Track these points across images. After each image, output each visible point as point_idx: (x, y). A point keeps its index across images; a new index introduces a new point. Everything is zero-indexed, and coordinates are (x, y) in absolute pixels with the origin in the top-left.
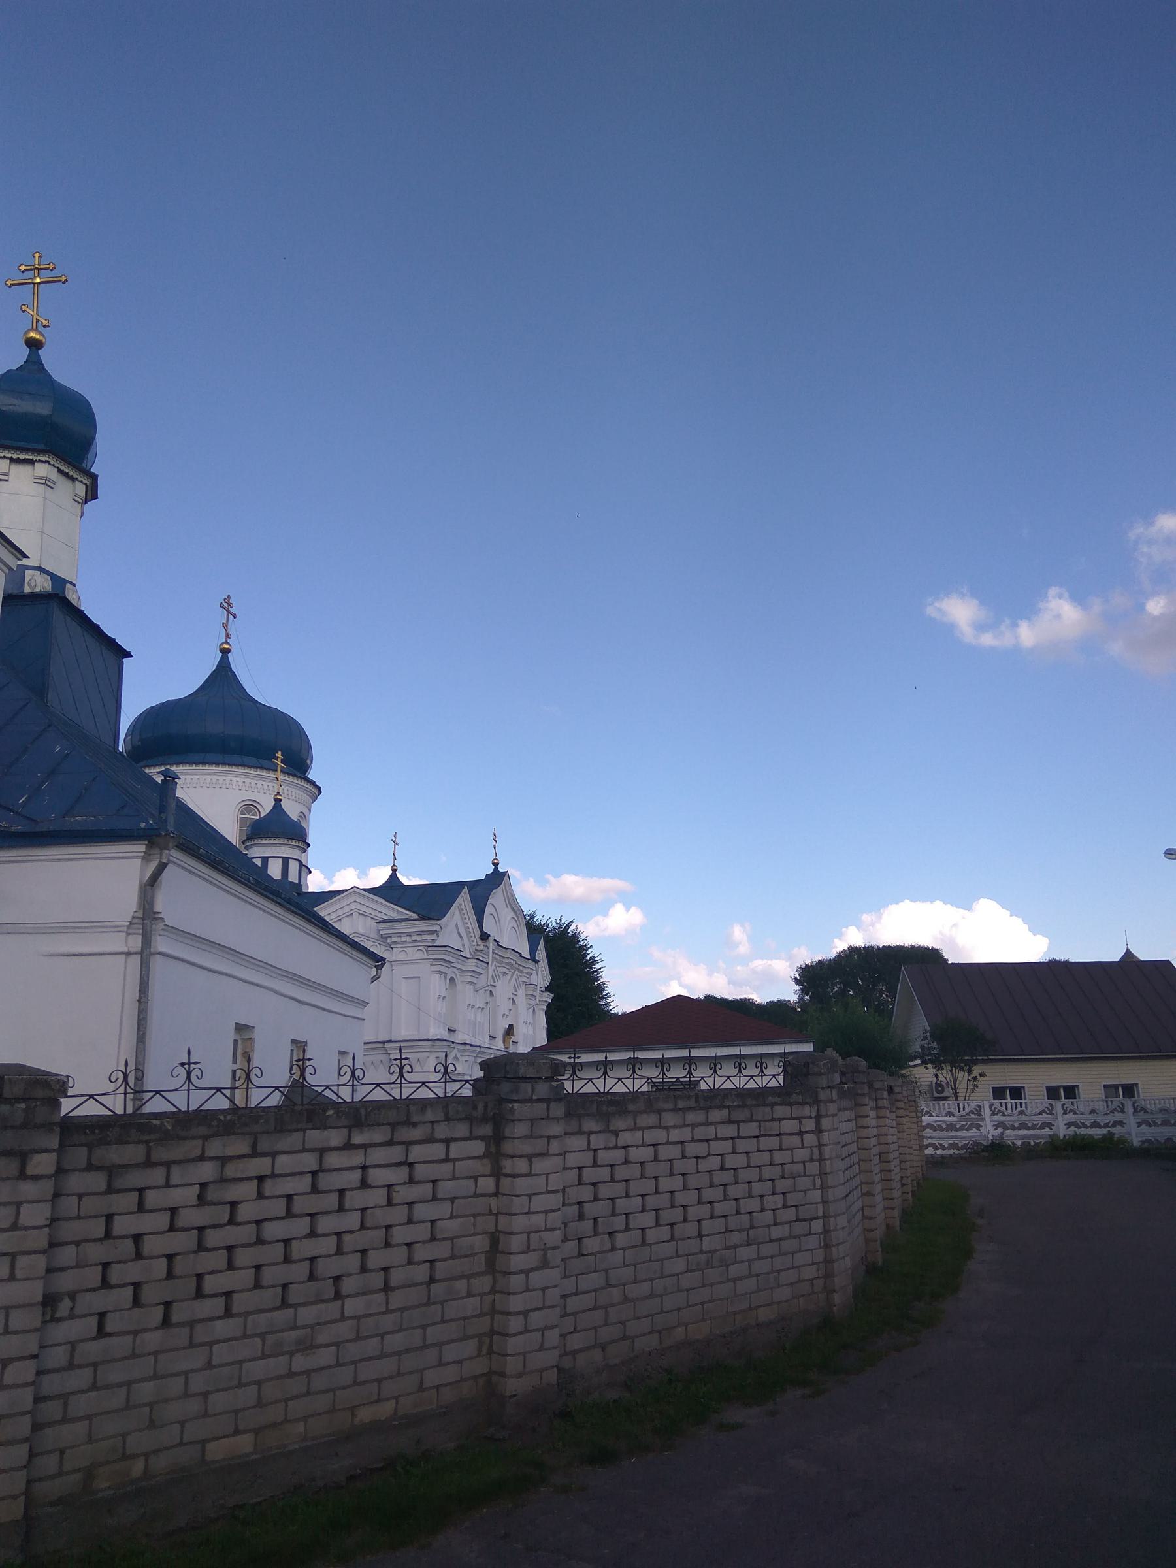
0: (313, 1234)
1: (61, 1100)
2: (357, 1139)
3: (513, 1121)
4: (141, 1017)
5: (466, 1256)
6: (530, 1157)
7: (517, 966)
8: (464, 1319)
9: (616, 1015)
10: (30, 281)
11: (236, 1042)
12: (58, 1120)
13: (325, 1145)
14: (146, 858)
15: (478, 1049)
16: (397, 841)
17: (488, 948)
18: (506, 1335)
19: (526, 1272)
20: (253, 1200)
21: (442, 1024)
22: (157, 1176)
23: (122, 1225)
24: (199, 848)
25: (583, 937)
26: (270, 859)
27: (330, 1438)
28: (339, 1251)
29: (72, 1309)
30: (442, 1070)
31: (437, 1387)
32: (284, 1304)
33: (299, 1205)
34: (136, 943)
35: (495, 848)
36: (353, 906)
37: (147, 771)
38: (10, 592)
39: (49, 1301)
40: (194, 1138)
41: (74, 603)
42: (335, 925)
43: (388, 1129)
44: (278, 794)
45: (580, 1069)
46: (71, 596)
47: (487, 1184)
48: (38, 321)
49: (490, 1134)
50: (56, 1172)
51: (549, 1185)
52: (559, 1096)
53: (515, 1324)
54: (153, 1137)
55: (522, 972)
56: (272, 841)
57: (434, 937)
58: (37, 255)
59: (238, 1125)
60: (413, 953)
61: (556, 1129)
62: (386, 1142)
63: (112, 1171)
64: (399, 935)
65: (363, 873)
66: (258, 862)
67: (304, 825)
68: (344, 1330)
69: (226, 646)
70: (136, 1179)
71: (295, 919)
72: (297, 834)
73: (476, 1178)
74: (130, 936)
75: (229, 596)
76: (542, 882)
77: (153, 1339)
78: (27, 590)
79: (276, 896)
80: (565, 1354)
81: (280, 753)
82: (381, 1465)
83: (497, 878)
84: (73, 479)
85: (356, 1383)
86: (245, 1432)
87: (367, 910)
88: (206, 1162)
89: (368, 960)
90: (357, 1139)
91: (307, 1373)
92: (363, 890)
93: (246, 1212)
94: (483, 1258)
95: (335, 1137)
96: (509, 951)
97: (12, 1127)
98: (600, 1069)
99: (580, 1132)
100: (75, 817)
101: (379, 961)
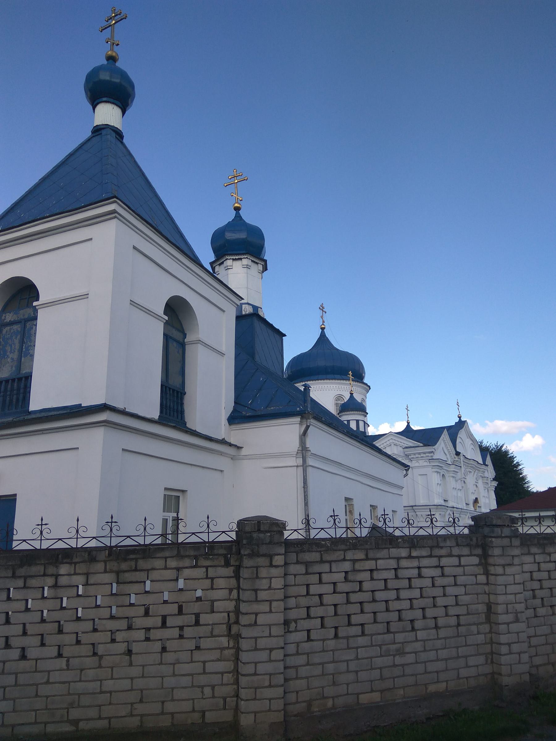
0: (398, 599)
1: (284, 532)
2: (414, 554)
3: (492, 547)
4: (305, 494)
5: (475, 614)
6: (504, 566)
7: (477, 468)
8: (477, 645)
9: (533, 492)
10: (233, 182)
11: (346, 506)
12: (283, 541)
13: (400, 556)
14: (301, 423)
15: (460, 510)
16: (408, 409)
17: (460, 459)
18: (501, 655)
19: (508, 624)
20: (369, 581)
21: (441, 497)
22: (325, 567)
23: (314, 589)
24: (322, 418)
25: (510, 452)
26: (350, 421)
27: (417, 698)
28: (412, 608)
29: (296, 627)
30: (452, 521)
31: (467, 678)
32: (388, 632)
33: (390, 584)
34: (300, 461)
35: (458, 409)
36: (391, 441)
37: (297, 385)
38: (237, 315)
39: (286, 623)
40: (340, 550)
41: (262, 316)
42: (384, 450)
43: (429, 549)
44: (351, 390)
45: (152, 527)
46: (261, 314)
47: (482, 579)
48: (238, 198)
49: (481, 553)
50: (285, 564)
51: (515, 580)
52: (516, 534)
53: (504, 649)
54: (323, 549)
55: (479, 471)
56: (351, 413)
57: (432, 454)
58: (235, 171)
59: (359, 545)
60: (422, 463)
61: (517, 552)
62: (428, 556)
63: (307, 564)
64: (415, 454)
65: (392, 425)
66: (346, 422)
67: (364, 404)
68: (418, 646)
69: (323, 326)
70: (317, 568)
71: (366, 448)
72: (361, 409)
73: (476, 576)
74: (298, 459)
75: (322, 304)
76: (484, 425)
77: (331, 644)
78: (244, 313)
79: (357, 438)
80: (532, 667)
81: (350, 372)
82: (441, 714)
83: (461, 424)
84: (257, 263)
85: (426, 672)
86: (376, 691)
87: (398, 443)
88: (346, 562)
89: (402, 467)
90: (414, 554)
91: (403, 665)
92: (395, 433)
93: (367, 586)
94: (484, 616)
95: (404, 553)
96: (471, 460)
97: (266, 544)
98: (537, 521)
99: (529, 553)
100: (271, 408)
101: (407, 467)
